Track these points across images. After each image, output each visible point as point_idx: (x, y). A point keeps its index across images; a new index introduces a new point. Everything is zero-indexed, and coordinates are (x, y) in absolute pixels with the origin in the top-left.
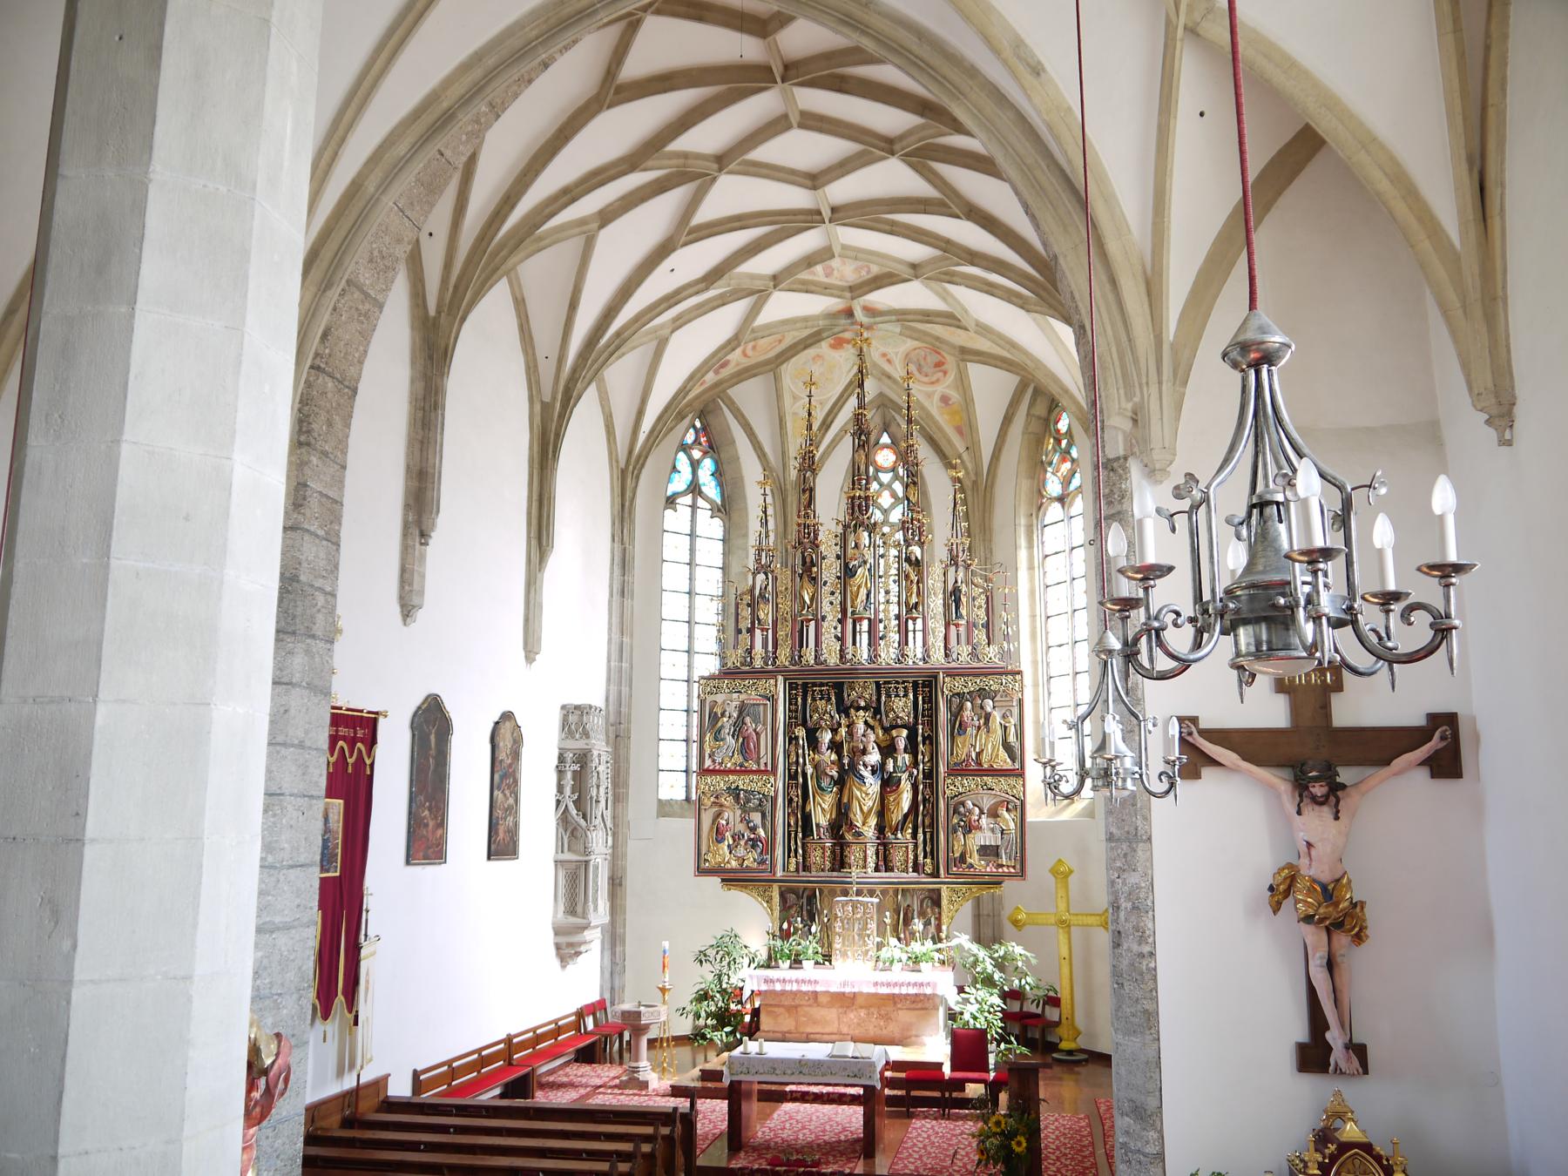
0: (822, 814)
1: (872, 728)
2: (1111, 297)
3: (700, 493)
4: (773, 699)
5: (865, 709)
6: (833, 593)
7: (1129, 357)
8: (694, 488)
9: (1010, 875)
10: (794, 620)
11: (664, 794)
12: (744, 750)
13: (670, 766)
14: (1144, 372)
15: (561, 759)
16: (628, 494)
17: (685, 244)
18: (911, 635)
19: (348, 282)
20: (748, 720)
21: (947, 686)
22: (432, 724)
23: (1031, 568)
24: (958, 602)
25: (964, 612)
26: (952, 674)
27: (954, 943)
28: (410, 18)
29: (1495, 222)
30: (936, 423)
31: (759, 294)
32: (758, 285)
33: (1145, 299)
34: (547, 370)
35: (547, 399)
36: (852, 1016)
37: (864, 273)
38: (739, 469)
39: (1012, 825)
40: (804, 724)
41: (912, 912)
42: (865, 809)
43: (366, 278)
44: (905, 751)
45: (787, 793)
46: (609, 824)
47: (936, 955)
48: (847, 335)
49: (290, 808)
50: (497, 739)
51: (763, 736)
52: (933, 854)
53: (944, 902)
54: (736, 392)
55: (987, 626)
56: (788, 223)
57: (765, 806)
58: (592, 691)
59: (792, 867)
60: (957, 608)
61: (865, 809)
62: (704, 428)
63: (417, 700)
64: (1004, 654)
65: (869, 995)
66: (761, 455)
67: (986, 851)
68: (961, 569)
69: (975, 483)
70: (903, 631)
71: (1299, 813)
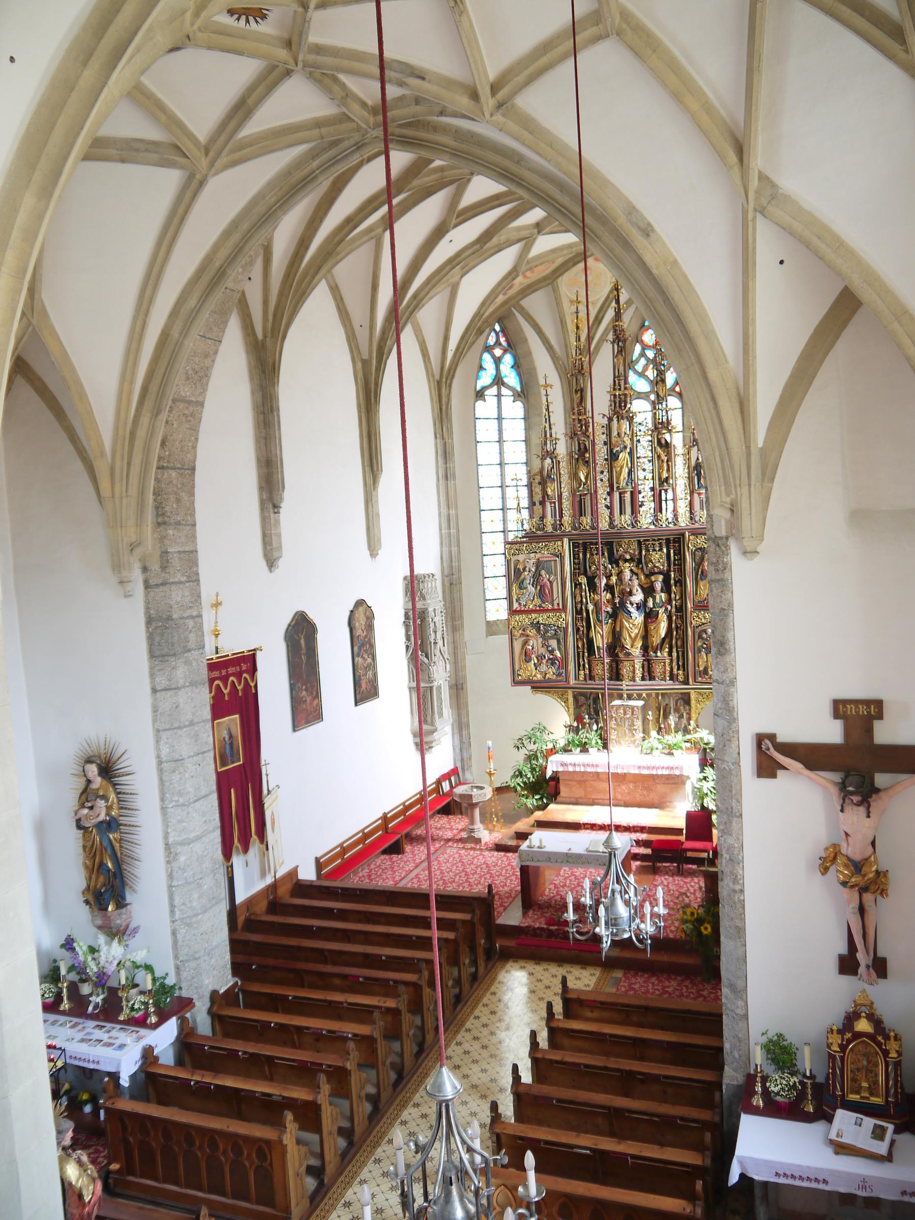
1: (637, 574)
2: (713, 412)
3: (503, 384)
4: (561, 556)
6: (602, 472)
7: (727, 462)
8: (498, 381)
11: (491, 617)
12: (541, 594)
14: (737, 473)
16: (444, 400)
17: (456, 226)
18: (664, 503)
20: (543, 572)
21: (692, 542)
22: (301, 635)
24: (699, 475)
26: (696, 533)
27: (698, 735)
28: (176, 220)
32: (524, 233)
34: (362, 336)
35: (366, 356)
36: (624, 788)
38: (532, 361)
41: (670, 710)
42: (633, 635)
43: (186, 392)
44: (662, 591)
45: (575, 625)
47: (684, 745)
49: (189, 765)
51: (555, 584)
52: (684, 667)
53: (693, 702)
54: (525, 303)
57: (560, 634)
59: (582, 677)
61: (633, 635)
62: (502, 330)
63: (286, 619)
65: (635, 775)
71: (842, 811)
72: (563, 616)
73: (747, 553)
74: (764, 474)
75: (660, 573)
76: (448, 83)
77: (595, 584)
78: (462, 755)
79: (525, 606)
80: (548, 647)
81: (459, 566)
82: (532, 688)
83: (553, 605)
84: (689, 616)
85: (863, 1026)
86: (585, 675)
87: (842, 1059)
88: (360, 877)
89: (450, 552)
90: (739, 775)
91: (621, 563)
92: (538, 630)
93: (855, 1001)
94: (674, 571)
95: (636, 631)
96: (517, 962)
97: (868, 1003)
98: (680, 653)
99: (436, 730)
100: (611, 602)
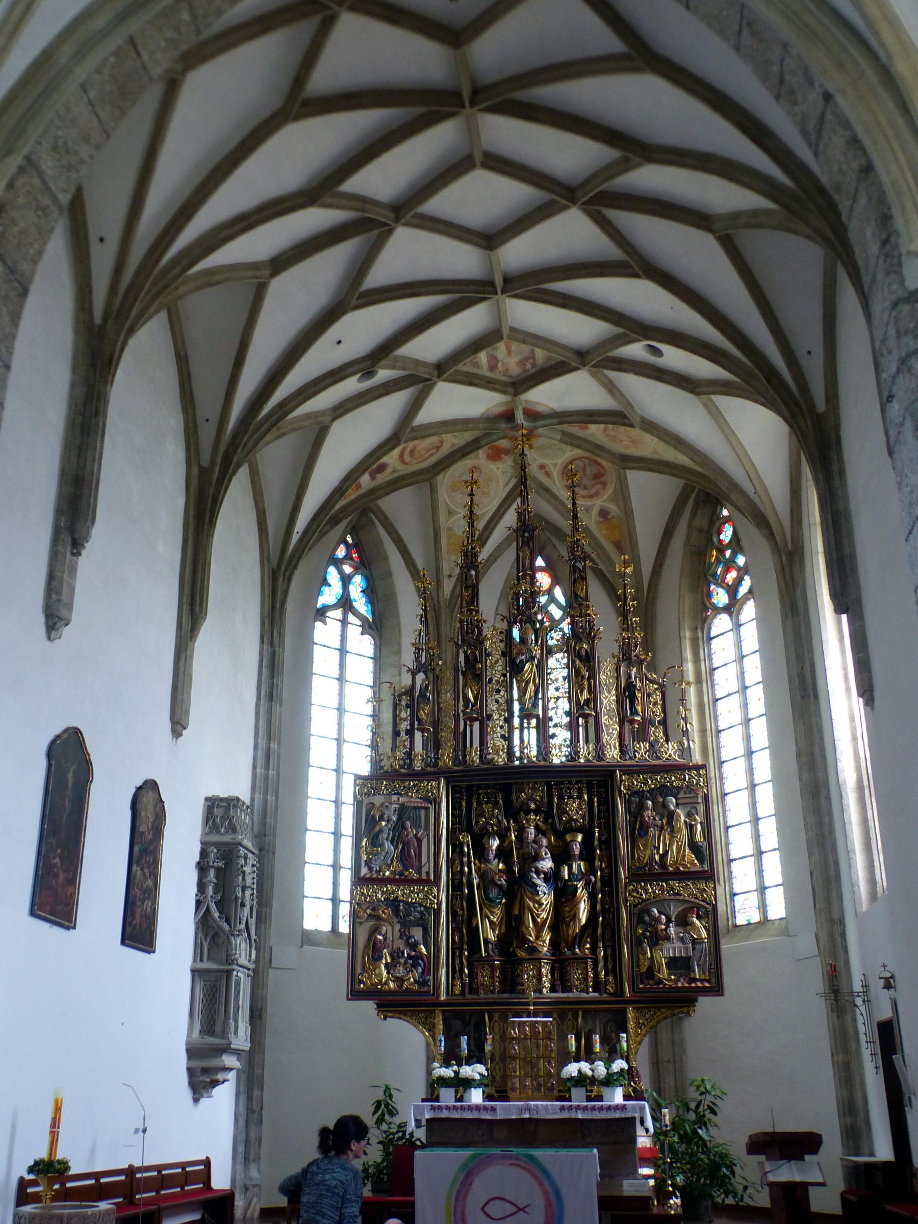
1: (544, 834)
8: (345, 603)
9: (705, 992)
12: (404, 858)
13: (323, 888)
15: (204, 854)
16: (279, 595)
19: (28, 159)
20: (408, 824)
21: (624, 783)
23: (699, 681)
24: (632, 698)
25: (639, 708)
26: (630, 771)
31: (421, 380)
35: (205, 463)
37: (529, 366)
39: (704, 934)
40: (469, 830)
48: (504, 443)
50: (139, 806)
54: (387, 503)
56: (463, 293)
58: (237, 783)
63: (57, 729)
66: (414, 573)
78: (247, 1133)
79: (378, 872)
82: (379, 1006)
83: (419, 871)
84: (621, 890)
89: (265, 802)
92: (396, 912)
95: (544, 915)
100: (509, 870)
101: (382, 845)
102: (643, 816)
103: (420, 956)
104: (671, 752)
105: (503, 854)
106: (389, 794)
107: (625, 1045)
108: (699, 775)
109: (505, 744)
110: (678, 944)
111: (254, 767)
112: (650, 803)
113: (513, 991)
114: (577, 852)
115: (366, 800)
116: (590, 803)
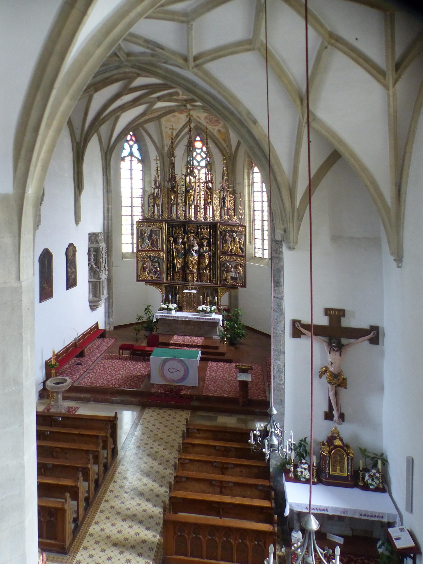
0: (178, 263)
1: (196, 239)
5: (193, 233)
8: (131, 154)
9: (241, 286)
10: (168, 205)
12: (152, 244)
13: (127, 243)
15: (89, 250)
16: (108, 160)
20: (153, 235)
21: (220, 228)
23: (249, 186)
24: (224, 202)
26: (223, 224)
29: (403, 195)
30: (216, 138)
33: (290, 198)
44: (207, 246)
46: (107, 268)
55: (234, 209)
57: (160, 261)
60: (224, 204)
64: (239, 219)
67: (232, 278)
68: (225, 191)
69: (229, 157)
70: (205, 209)
71: (330, 353)
72: (162, 253)
73: (291, 248)
74: (298, 219)
75: (206, 239)
76: (174, 53)
77: (177, 241)
79: (144, 248)
80: (154, 266)
81: (112, 229)
83: (157, 248)
85: (337, 442)
86: (171, 278)
87: (330, 457)
88: (65, 369)
90: (284, 336)
91: (189, 234)
92: (150, 259)
93: (332, 432)
94: (212, 239)
95: (195, 262)
96: (150, 408)
97: (337, 432)
98: (214, 272)
99: (101, 300)
100: (184, 249)
101: (145, 241)
102: (226, 238)
103: (158, 271)
104: (235, 219)
105: (183, 243)
106: (147, 226)
107: (217, 300)
108: (243, 229)
109: (184, 213)
110: (234, 273)
111: (104, 213)
112: (228, 234)
113: (186, 281)
114: (206, 245)
115: (140, 228)
116: (210, 232)
